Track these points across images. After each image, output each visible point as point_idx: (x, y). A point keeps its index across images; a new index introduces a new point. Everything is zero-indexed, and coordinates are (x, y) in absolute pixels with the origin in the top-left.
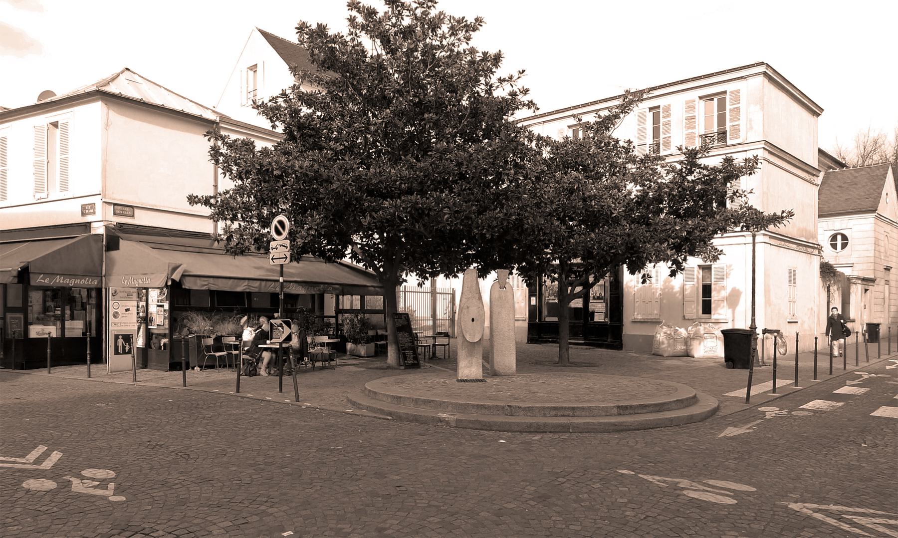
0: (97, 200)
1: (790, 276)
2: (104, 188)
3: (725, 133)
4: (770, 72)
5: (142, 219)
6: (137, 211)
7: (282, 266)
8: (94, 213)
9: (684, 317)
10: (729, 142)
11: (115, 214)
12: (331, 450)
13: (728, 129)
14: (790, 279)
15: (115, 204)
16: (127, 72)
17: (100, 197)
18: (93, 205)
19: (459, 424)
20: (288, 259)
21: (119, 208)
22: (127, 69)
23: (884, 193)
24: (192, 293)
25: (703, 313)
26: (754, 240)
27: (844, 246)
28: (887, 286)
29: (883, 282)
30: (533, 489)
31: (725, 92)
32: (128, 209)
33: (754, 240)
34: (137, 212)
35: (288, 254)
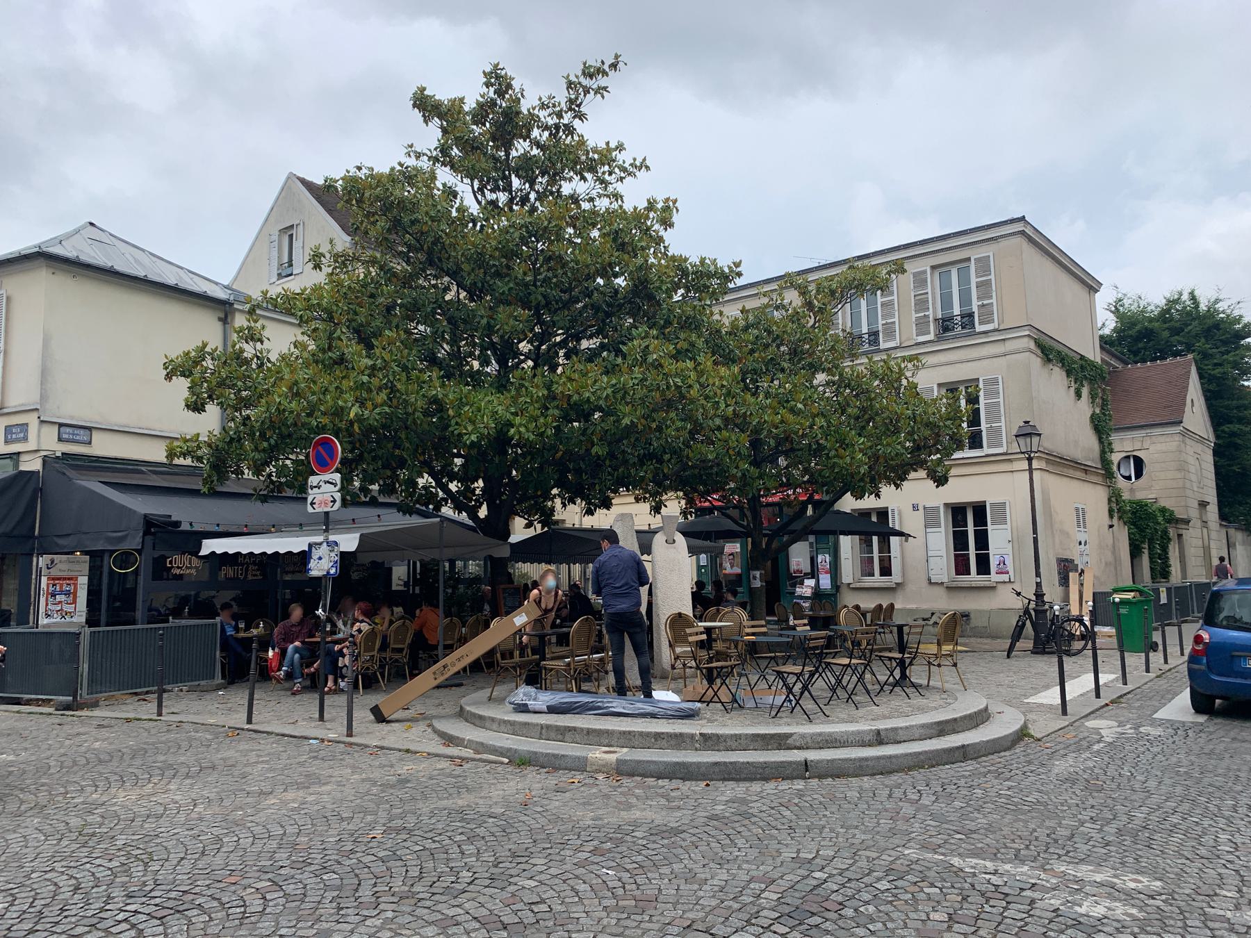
0: (32, 420)
1: (1078, 516)
2: (44, 397)
3: (971, 315)
4: (1029, 231)
5: (103, 446)
6: (95, 435)
7: (327, 513)
8: (25, 439)
9: (929, 580)
10: (979, 328)
11: (60, 439)
12: (410, 832)
13: (975, 309)
14: (1078, 522)
15: (61, 425)
16: (91, 228)
17: (35, 415)
18: (24, 427)
19: (623, 770)
20: (338, 504)
21: (68, 430)
22: (92, 224)
23: (1188, 402)
24: (972, 616)
25: (881, 575)
26: (1030, 465)
27: (1139, 474)
28: (1205, 530)
29: (1199, 524)
30: (775, 897)
31: (969, 259)
32: (82, 432)
33: (1030, 465)
34: (96, 436)
35: (338, 496)
